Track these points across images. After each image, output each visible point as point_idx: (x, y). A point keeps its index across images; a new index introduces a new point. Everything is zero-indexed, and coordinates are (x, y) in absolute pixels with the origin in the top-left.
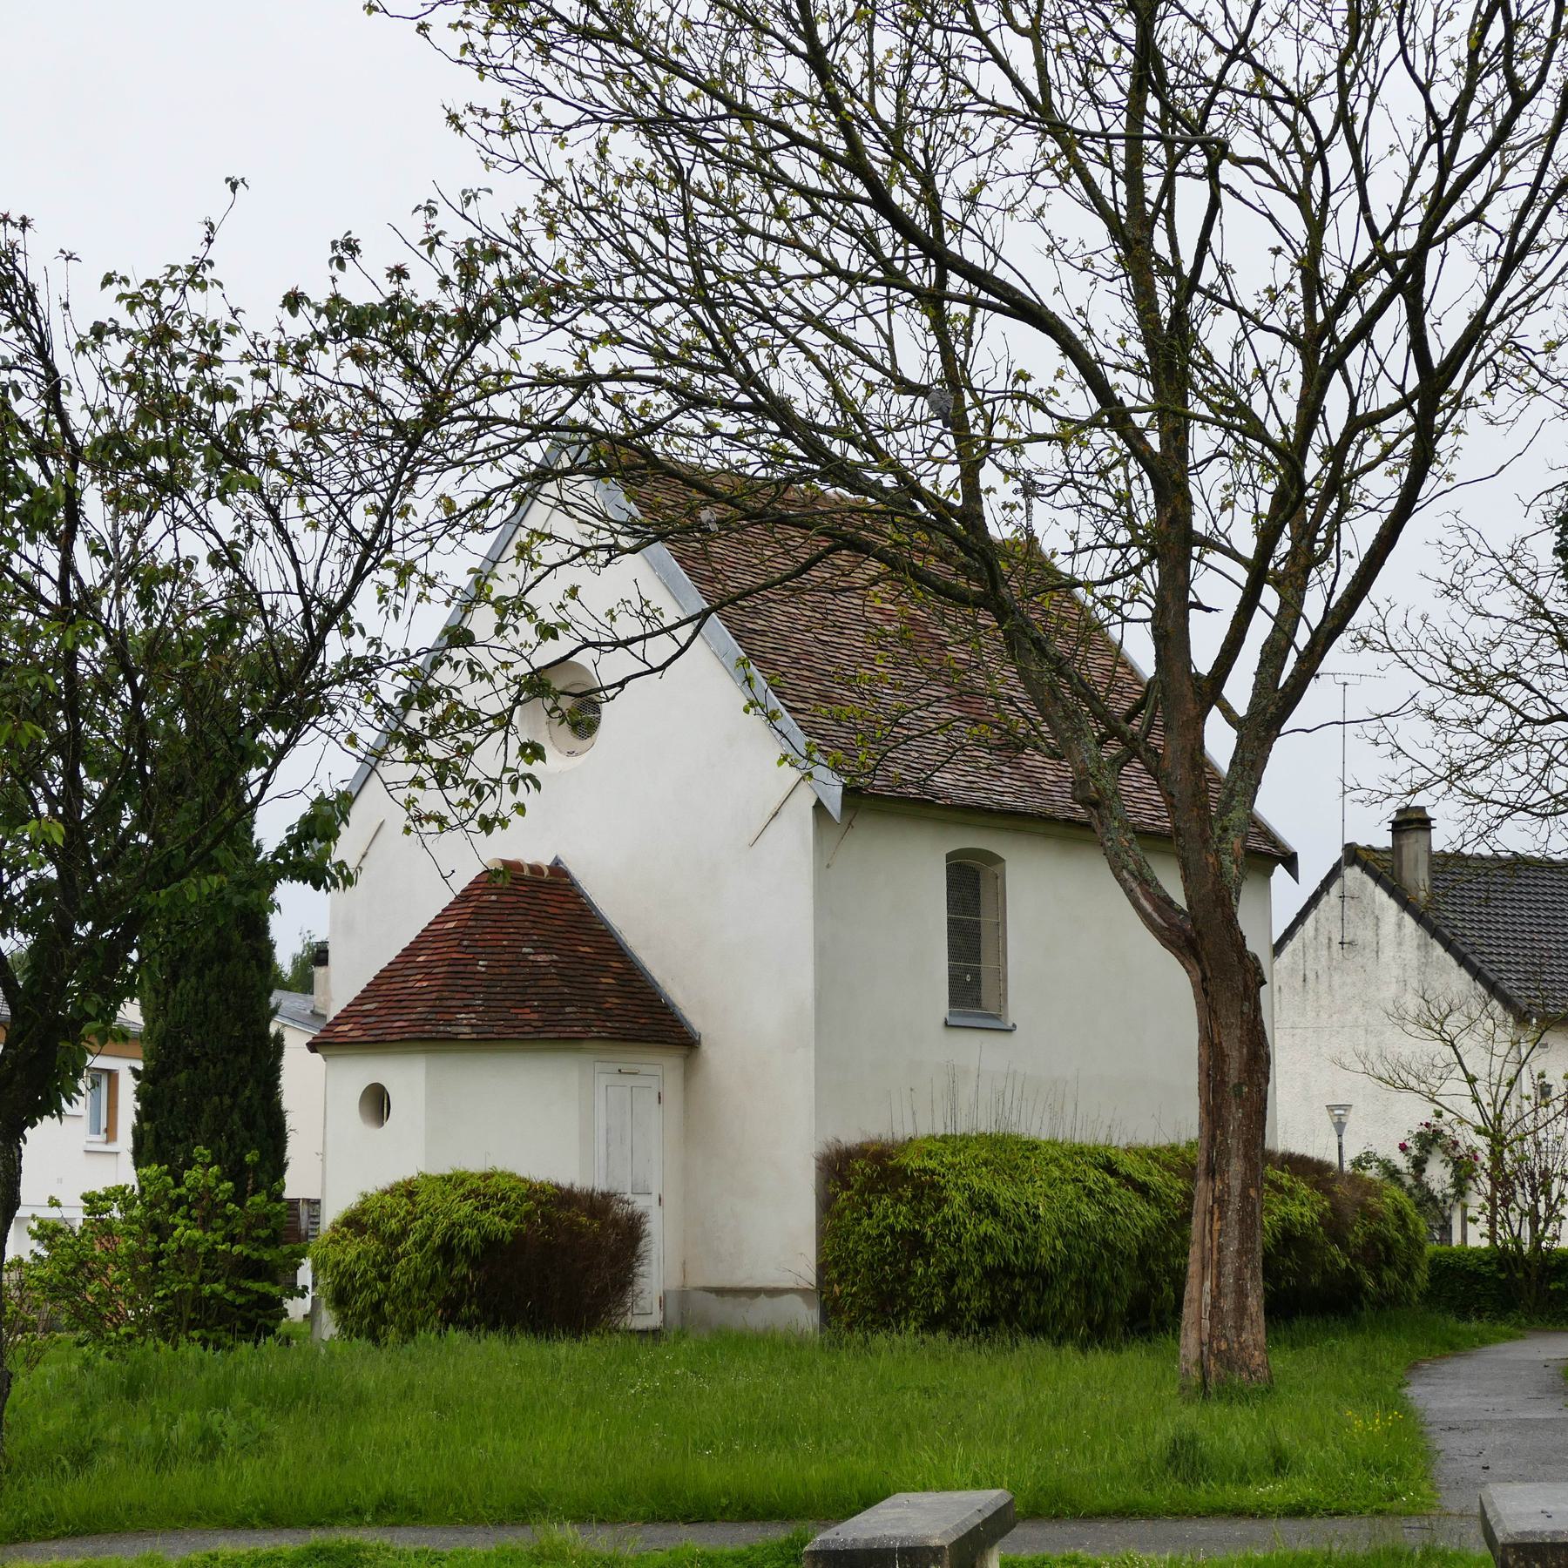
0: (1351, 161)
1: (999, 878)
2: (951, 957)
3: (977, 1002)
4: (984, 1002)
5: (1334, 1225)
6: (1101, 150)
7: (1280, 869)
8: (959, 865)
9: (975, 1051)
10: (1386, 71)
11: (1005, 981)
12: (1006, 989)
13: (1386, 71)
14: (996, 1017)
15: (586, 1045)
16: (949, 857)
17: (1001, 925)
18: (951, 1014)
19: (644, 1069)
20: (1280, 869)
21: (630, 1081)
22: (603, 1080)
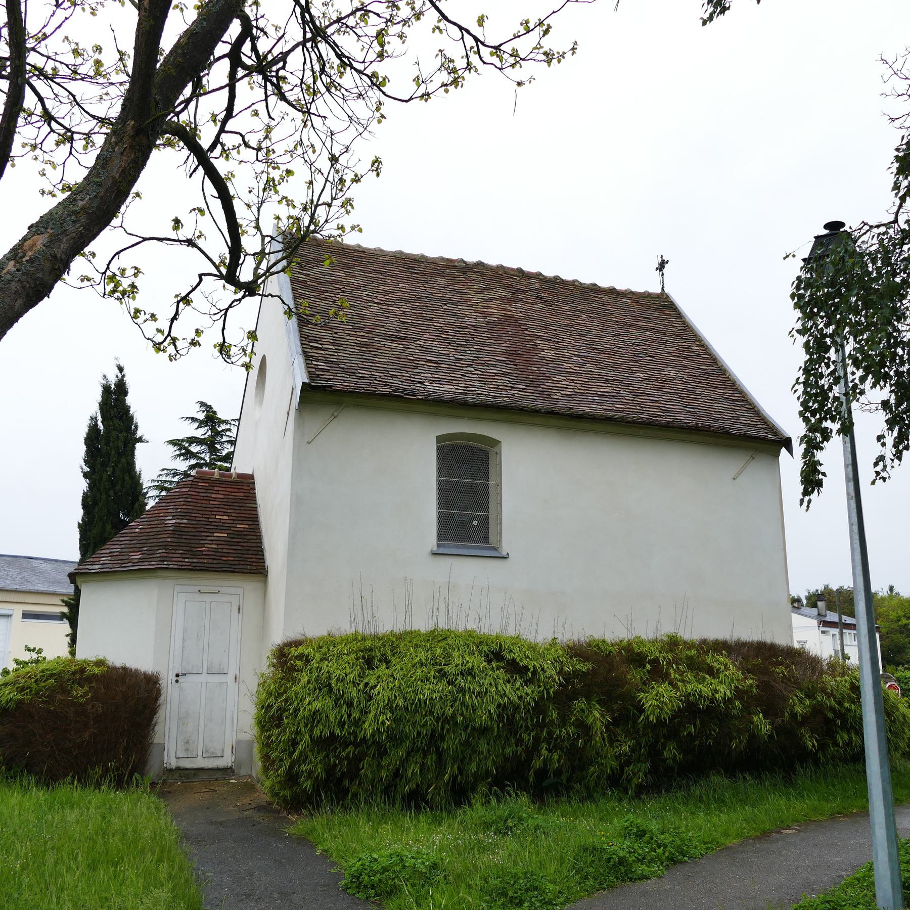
0: (226, 105)
1: (498, 454)
2: (440, 505)
3: (486, 539)
4: (491, 540)
5: (768, 700)
6: (275, 81)
7: (784, 451)
8: (454, 448)
9: (468, 572)
10: (305, 63)
11: (501, 523)
12: (501, 530)
13: (305, 63)
14: (495, 549)
15: (160, 573)
16: (439, 439)
17: (499, 485)
18: (438, 546)
19: (222, 590)
20: (784, 451)
21: (208, 598)
22: (182, 598)
